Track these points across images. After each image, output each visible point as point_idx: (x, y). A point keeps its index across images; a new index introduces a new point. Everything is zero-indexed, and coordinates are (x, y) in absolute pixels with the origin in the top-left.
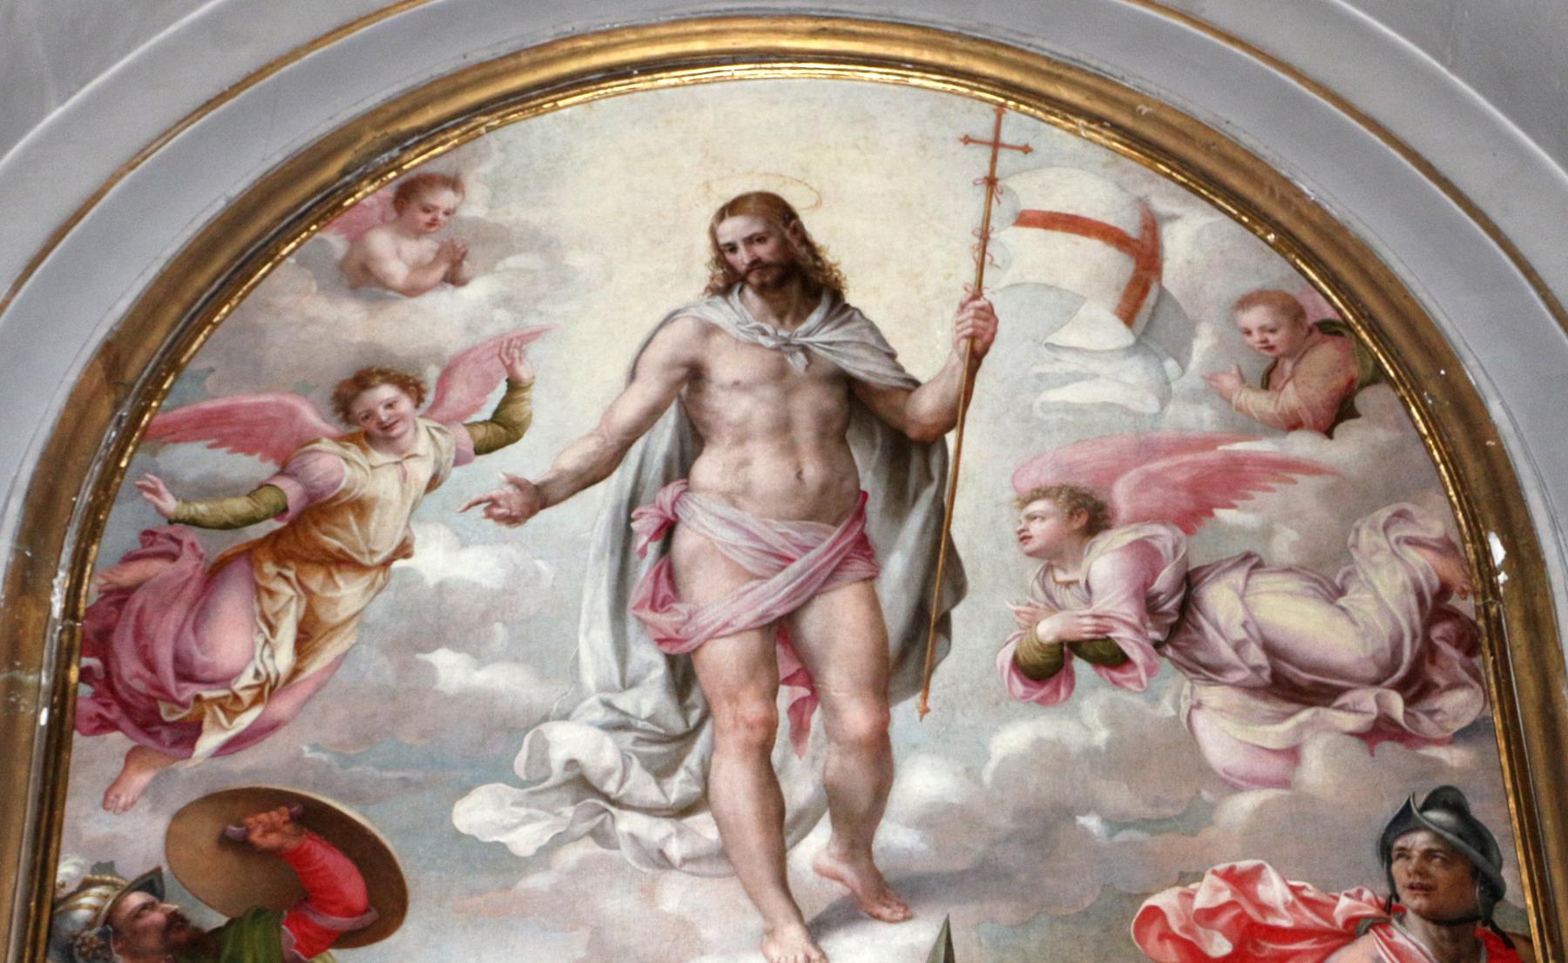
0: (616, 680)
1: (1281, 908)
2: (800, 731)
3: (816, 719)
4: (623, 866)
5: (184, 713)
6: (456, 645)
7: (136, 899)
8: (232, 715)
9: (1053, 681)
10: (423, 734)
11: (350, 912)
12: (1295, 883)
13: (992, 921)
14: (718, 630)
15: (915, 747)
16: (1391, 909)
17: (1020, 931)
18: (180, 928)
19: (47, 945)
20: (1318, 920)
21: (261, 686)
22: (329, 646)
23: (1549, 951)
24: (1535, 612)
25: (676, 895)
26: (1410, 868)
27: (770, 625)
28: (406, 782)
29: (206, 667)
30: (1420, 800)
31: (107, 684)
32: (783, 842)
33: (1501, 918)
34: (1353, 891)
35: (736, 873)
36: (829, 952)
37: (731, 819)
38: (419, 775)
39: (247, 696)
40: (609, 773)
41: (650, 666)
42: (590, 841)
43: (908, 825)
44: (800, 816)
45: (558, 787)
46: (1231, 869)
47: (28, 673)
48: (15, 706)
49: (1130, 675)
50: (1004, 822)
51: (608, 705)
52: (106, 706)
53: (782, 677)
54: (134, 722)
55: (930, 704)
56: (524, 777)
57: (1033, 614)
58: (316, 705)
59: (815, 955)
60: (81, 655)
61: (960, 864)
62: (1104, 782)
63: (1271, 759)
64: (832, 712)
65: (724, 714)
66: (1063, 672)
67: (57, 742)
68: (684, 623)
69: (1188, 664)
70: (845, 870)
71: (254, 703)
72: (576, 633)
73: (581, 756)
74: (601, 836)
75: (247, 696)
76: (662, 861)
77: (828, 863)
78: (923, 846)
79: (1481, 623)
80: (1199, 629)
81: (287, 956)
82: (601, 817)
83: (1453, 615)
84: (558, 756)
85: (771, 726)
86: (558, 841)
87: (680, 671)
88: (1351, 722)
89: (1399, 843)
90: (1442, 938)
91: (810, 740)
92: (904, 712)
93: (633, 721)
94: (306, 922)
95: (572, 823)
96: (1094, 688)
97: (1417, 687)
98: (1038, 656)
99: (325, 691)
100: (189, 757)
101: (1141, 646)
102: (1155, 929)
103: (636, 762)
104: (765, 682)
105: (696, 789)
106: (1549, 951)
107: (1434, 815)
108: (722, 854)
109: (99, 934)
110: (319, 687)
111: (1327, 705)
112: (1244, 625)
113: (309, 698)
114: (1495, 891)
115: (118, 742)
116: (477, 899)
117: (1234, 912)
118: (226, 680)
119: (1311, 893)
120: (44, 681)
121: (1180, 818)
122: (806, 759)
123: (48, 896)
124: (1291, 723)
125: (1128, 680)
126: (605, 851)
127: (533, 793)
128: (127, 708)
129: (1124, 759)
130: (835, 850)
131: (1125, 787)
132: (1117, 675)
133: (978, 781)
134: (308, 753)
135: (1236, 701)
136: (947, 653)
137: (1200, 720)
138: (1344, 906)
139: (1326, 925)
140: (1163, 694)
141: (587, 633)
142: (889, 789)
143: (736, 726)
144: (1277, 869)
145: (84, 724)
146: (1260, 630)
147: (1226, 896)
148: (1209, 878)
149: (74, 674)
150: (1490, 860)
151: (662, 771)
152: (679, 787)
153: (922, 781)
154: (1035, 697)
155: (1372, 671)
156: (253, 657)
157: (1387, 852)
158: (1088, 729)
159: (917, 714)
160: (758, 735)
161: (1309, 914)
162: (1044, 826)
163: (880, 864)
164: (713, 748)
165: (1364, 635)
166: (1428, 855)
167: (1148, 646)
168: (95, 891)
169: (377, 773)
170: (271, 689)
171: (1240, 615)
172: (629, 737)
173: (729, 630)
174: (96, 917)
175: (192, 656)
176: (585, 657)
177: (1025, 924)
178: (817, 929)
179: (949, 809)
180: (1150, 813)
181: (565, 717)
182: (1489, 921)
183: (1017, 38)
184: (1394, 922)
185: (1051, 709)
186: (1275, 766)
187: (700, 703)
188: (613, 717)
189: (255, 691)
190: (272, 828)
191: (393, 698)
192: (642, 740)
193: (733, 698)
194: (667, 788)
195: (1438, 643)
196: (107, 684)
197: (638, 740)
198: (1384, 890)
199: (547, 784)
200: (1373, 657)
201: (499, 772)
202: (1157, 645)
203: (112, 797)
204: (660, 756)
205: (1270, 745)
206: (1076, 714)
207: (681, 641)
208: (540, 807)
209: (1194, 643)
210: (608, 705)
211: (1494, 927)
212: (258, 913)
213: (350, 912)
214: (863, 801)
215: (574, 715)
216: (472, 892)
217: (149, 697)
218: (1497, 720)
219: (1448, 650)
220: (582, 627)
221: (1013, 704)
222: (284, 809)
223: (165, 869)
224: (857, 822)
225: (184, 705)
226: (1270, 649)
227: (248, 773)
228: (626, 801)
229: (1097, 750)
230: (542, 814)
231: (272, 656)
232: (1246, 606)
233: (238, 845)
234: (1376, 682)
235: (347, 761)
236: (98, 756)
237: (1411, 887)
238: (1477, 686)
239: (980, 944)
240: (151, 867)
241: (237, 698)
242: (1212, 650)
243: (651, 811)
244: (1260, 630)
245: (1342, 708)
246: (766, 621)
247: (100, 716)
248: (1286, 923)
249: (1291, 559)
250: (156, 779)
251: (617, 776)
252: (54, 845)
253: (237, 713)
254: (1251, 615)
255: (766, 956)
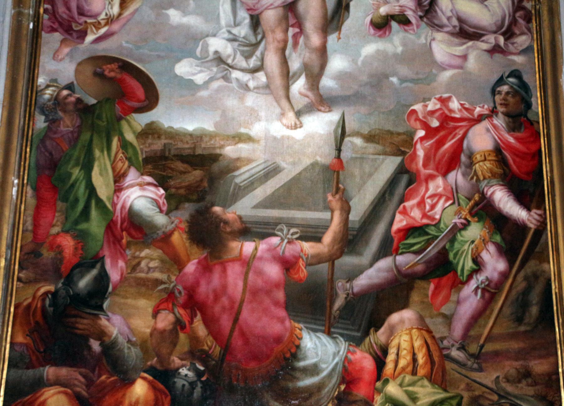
0: (232, 23)
1: (457, 111)
2: (296, 44)
3: (301, 40)
4: (232, 90)
5: (81, 27)
6: (177, 8)
7: (65, 92)
8: (98, 29)
9: (384, 29)
10: (165, 40)
11: (139, 101)
12: (462, 102)
13: (359, 112)
14: (269, 6)
15: (335, 51)
16: (493, 112)
17: (368, 117)
18: (80, 103)
19: (35, 107)
20: (469, 115)
21: (108, 19)
22: (132, 6)
23: (545, 126)
24: (552, 8)
25: (251, 100)
26: (501, 98)
27: (287, 5)
28: (159, 56)
29: (89, 11)
30: (507, 74)
31: (54, 14)
32: (288, 83)
33: (530, 115)
34: (481, 105)
35: (272, 93)
36: (303, 122)
37: (271, 75)
38: (163, 54)
39: (103, 22)
40: (229, 56)
41: (244, 19)
42: (222, 80)
43: (332, 78)
44: (295, 74)
45: (211, 61)
46: (441, 97)
47: (25, 10)
48: (21, 21)
49: (411, 28)
50: (364, 78)
51: (229, 32)
52: (54, 23)
53: (290, 24)
54: (63, 29)
55: (341, 36)
56: (199, 56)
57: (379, 5)
58: (127, 27)
60: (44, 4)
61: (348, 93)
62: (399, 66)
63: (457, 59)
64: (307, 38)
65: (270, 37)
66: (388, 26)
67: (36, 35)
68: (257, 3)
69: (430, 24)
70: (309, 94)
71: (105, 25)
72: (219, 5)
73: (220, 50)
74: (226, 78)
75: (103, 22)
76: (246, 88)
77: (304, 91)
78: (336, 86)
79: (533, 12)
80: (436, 12)
82: (226, 72)
83: (524, 8)
84: (212, 49)
85: (286, 42)
86: (212, 79)
87: (254, 21)
88: (485, 46)
89: (498, 89)
90: (510, 122)
91: (299, 47)
92: (332, 39)
93: (237, 38)
94: (124, 104)
95: (216, 73)
96: (398, 32)
97: (509, 34)
98: (379, 20)
99: (130, 22)
100: (82, 43)
101: (415, 18)
102: (413, 117)
103: (238, 53)
104: (284, 26)
105: (259, 63)
106: (545, 126)
107: (511, 80)
108: (267, 86)
109: (53, 104)
110: (128, 21)
111: (478, 40)
112: (451, 11)
113: (124, 25)
114: (529, 106)
115: (57, 36)
116: (183, 99)
117: (440, 112)
118: (95, 16)
119: (467, 106)
120: (31, 12)
121: (425, 79)
122: (298, 54)
123: (35, 89)
124: (465, 47)
125: (410, 30)
126: (227, 84)
127: (203, 62)
128: (61, 24)
129: (407, 58)
130: (306, 87)
131: (406, 68)
132: (406, 28)
133: (356, 64)
134: (124, 44)
135: (447, 38)
136: (348, 17)
137: (434, 45)
138: (478, 110)
139: (471, 116)
140: (421, 35)
141: (222, 5)
142: (326, 65)
143: (274, 41)
144: (456, 97)
145: (45, 29)
146: (457, 13)
147: (438, 106)
148: (433, 100)
149: (42, 11)
150: (528, 95)
151: (247, 57)
152: (253, 62)
153: (337, 63)
154: (377, 35)
155: (494, 29)
156: (105, 8)
157: (494, 92)
158: (395, 47)
159: (336, 40)
160: (281, 45)
161: (466, 113)
162: (378, 80)
163: (322, 92)
164: (265, 49)
165: (492, 15)
166: (507, 93)
167: (418, 17)
168: (51, 88)
169: (149, 53)
170: (112, 20)
171: (450, 7)
172: (236, 44)
173: (273, 7)
174: (52, 98)
175: (83, 6)
176: (222, 15)
177: (370, 114)
178: (299, 114)
179: (346, 73)
180: (415, 77)
181: (214, 35)
182: (526, 116)
184: (494, 116)
185: (382, 39)
186: (458, 62)
187: (261, 33)
188: (231, 36)
189: (105, 21)
190: (112, 70)
191: (154, 26)
192: (241, 45)
193: (273, 31)
194: (249, 62)
195: (518, 18)
196: (54, 14)
197: (240, 45)
198: (492, 105)
199: (207, 59)
200: (495, 23)
201: (191, 54)
202: (421, 17)
203: (56, 56)
204: (247, 51)
205: (457, 54)
206: (391, 41)
207: (255, 10)
208: (205, 67)
209: (434, 17)
210: (229, 32)
211: (527, 119)
212: (108, 100)
213: (139, 101)
214: (316, 70)
215: (218, 35)
216: (181, 96)
217: (69, 21)
218: (535, 46)
219: (521, 21)
220: (221, 3)
221: (370, 37)
222: (116, 64)
223: (75, 83)
224: (314, 76)
225: (81, 24)
226: (460, 20)
227: (104, 50)
228: (235, 66)
229: (398, 54)
230: (206, 70)
231: (112, 8)
232: (452, 4)
233: (100, 75)
234: (495, 32)
235: (139, 48)
236: (51, 41)
237: (501, 104)
238: (529, 34)
239: (354, 121)
240: (70, 82)
241: (99, 23)
242: (440, 20)
243: (243, 70)
244: (457, 13)
245: (483, 41)
246: (285, 4)
247: (51, 26)
248: (458, 116)
249: (397, 263)
250: (71, 50)
251: (232, 58)
252: (36, 71)
253: (100, 28)
254: (454, 7)
255: (281, 122)
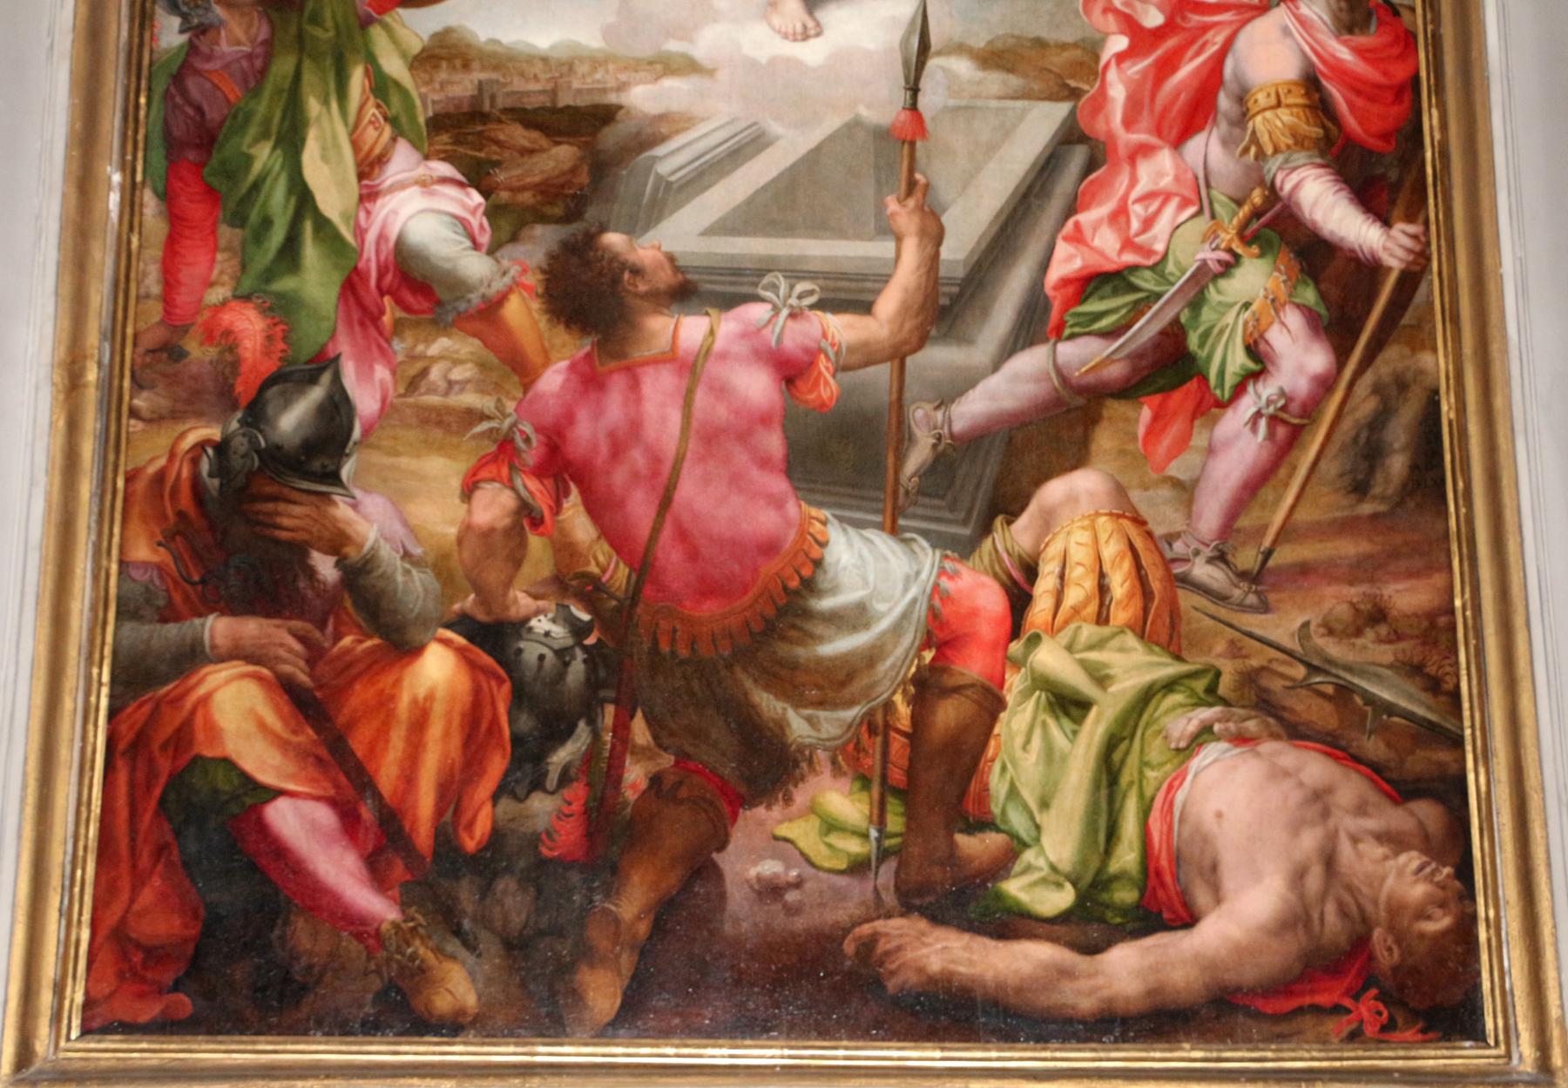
59: (810, 24)
81: (360, 12)
183: (982, 490)
223: (1463, 1056)
255: (770, 24)
